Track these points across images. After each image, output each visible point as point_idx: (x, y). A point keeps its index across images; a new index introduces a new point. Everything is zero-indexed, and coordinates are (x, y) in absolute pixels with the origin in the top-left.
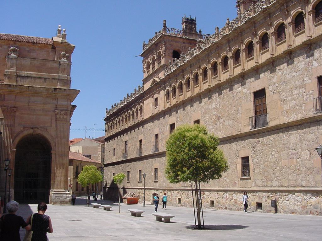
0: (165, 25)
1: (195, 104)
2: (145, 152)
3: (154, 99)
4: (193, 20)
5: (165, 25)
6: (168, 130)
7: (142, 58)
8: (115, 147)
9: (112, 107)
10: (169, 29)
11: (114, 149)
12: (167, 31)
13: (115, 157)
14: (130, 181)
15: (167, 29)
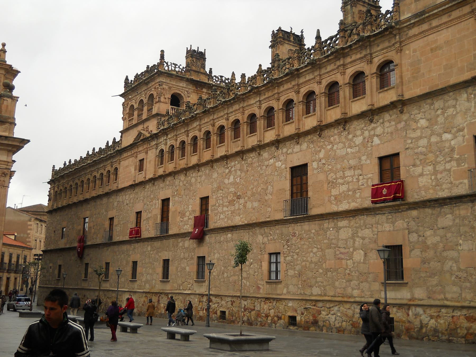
0: (162, 56)
2: (118, 237)
5: (162, 56)
7: (123, 100)
9: (65, 164)
10: (167, 63)
12: (165, 66)
13: (64, 241)
15: (165, 63)
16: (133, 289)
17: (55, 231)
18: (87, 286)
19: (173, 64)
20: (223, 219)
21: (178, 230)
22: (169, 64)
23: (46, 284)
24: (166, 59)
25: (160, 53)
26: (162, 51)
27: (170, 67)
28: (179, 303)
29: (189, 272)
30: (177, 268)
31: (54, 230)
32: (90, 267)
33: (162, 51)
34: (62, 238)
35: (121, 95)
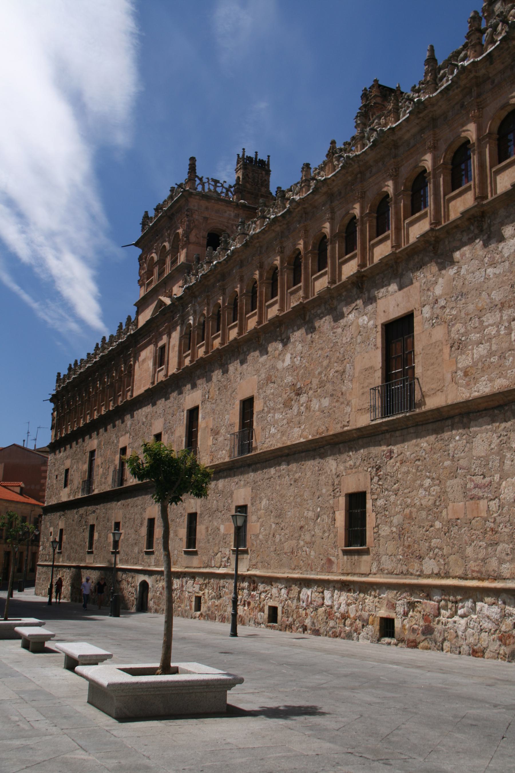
1: (101, 431)
3: (158, 348)
4: (262, 162)
6: (183, 423)
8: (68, 463)
11: (67, 471)
14: (94, 550)
16: (149, 566)
17: (57, 476)
18: (92, 561)
19: (213, 180)
20: (273, 435)
21: (209, 460)
22: (205, 180)
23: (46, 560)
24: (199, 173)
25: (188, 162)
26: (193, 160)
27: (206, 185)
28: (210, 591)
29: (224, 535)
30: (207, 528)
31: (56, 473)
32: (97, 531)
33: (193, 160)
34: (66, 485)
35: (137, 244)
